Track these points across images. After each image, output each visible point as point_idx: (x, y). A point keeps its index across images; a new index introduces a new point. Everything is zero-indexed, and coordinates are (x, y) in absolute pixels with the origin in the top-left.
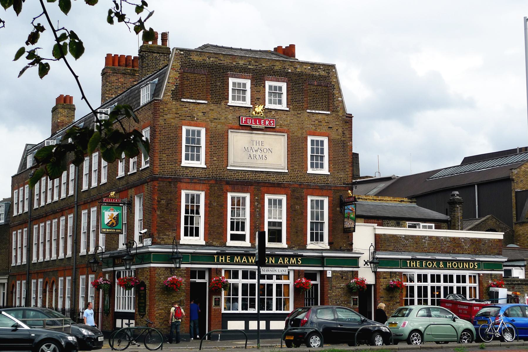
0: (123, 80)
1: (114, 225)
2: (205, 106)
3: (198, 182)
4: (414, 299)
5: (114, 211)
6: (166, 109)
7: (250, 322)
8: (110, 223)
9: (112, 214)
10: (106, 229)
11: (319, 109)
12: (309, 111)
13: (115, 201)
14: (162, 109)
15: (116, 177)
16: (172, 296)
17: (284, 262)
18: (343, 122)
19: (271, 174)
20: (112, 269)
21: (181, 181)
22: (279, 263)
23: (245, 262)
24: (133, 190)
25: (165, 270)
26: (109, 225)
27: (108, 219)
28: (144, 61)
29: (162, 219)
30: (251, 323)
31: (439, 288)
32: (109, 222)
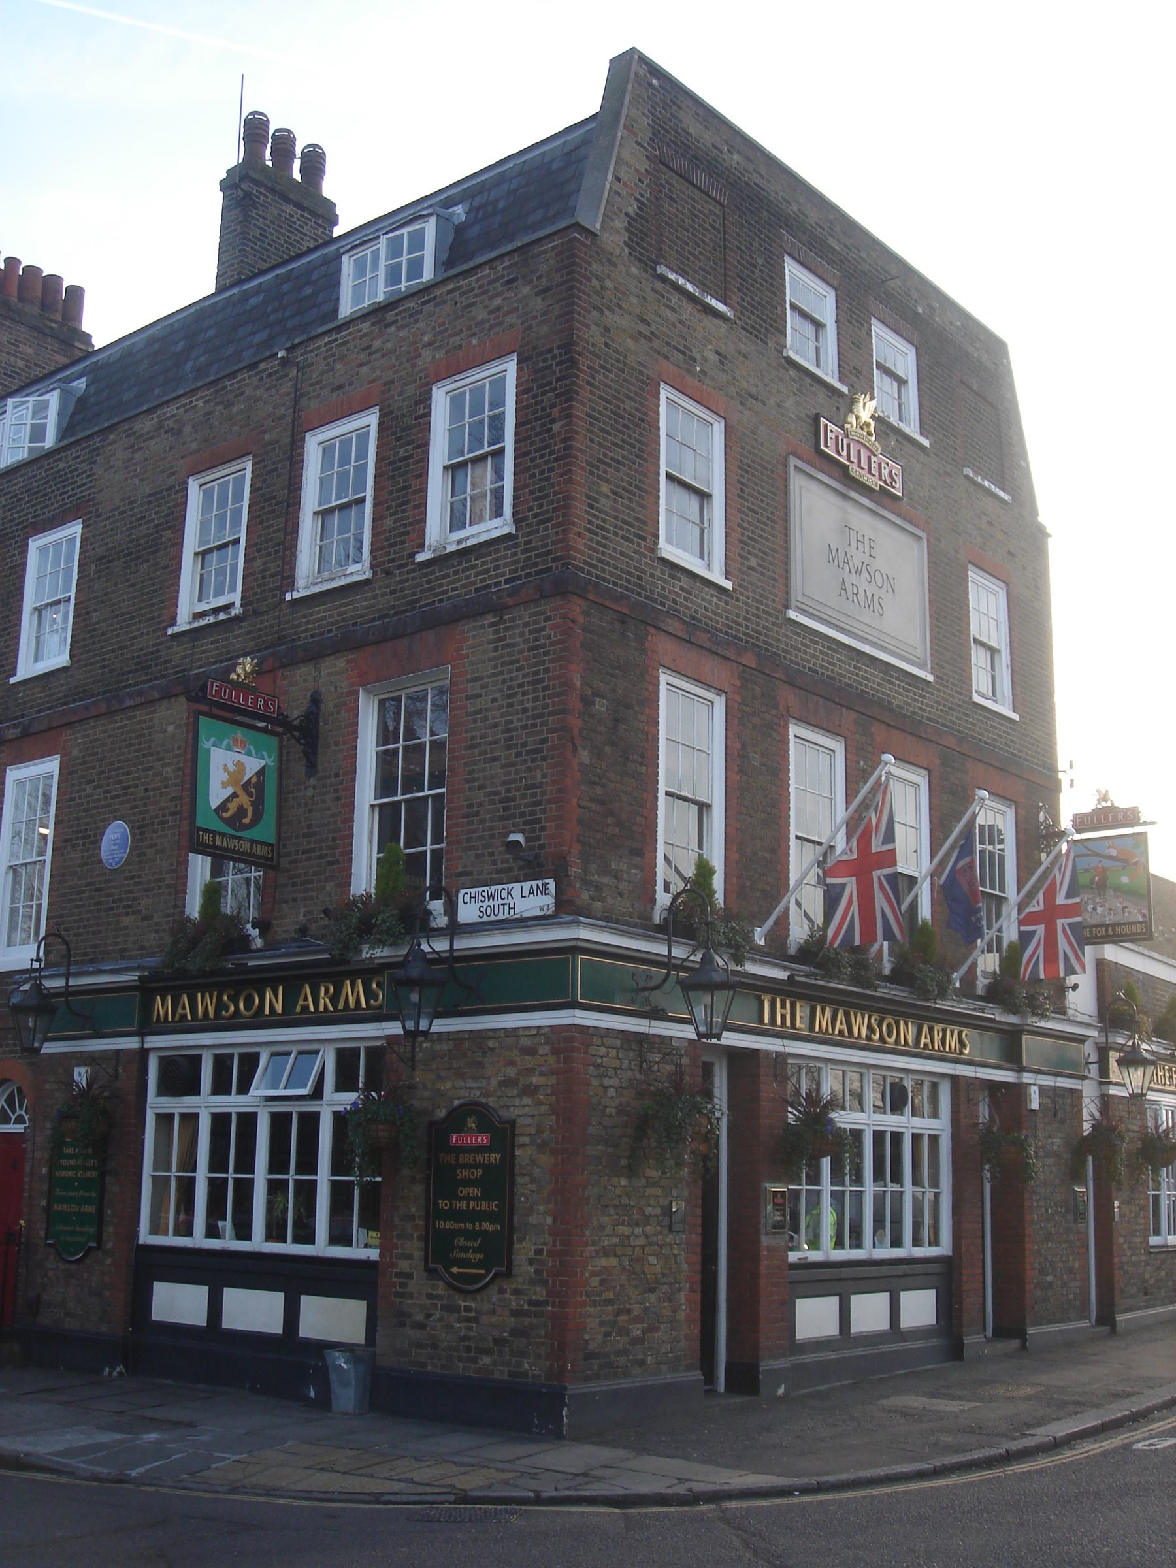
0: (30, 351)
1: (246, 821)
2: (724, 327)
3: (707, 645)
5: (249, 754)
6: (609, 284)
8: (230, 805)
9: (240, 766)
10: (214, 832)
11: (991, 477)
12: (968, 472)
13: (255, 702)
14: (597, 277)
15: (166, 628)
16: (643, 1181)
19: (892, 676)
20: (132, 1043)
21: (661, 625)
24: (340, 663)
25: (622, 1047)
26: (226, 815)
27: (224, 785)
28: (253, 218)
29: (598, 790)
30: (859, 1302)
31: (190, 1119)
32: (227, 800)
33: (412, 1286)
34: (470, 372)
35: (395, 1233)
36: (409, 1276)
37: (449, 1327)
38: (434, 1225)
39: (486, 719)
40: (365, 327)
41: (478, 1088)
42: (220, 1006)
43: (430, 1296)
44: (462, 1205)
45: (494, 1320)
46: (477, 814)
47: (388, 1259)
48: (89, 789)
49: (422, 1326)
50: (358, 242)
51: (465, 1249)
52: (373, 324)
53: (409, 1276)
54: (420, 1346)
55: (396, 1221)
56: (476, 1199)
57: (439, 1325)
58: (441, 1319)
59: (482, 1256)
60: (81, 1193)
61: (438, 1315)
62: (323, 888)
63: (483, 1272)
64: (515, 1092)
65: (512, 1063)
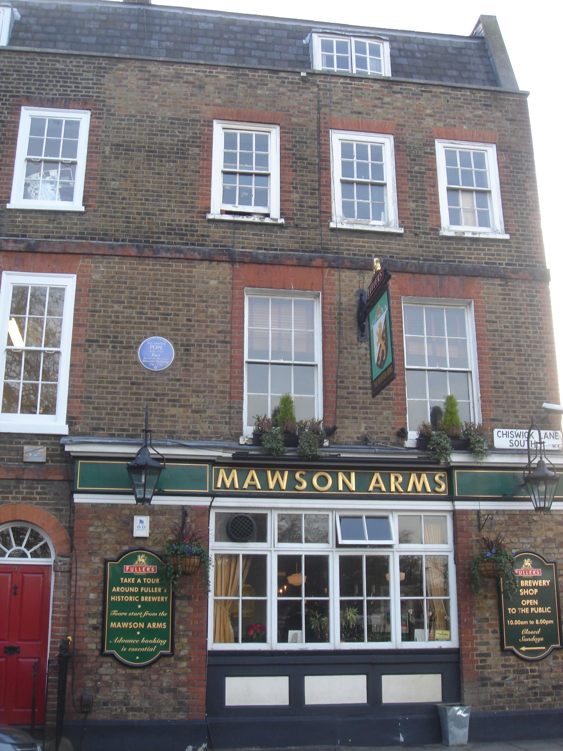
4: (342, 594)
7: (385, 678)
17: (388, 486)
18: (523, 214)
22: (371, 488)
23: (255, 486)
33: (490, 661)
34: (462, 142)
35: (474, 630)
36: (488, 655)
37: (520, 683)
38: (506, 623)
39: (502, 336)
40: (377, 86)
41: (529, 543)
42: (293, 482)
43: (504, 666)
44: (526, 610)
45: (552, 675)
46: (502, 387)
47: (470, 646)
48: (116, 307)
49: (500, 685)
50: (328, 31)
51: (527, 636)
52: (382, 87)
53: (488, 655)
54: (500, 696)
55: (475, 622)
56: (535, 606)
57: (513, 683)
58: (514, 679)
59: (542, 639)
60: (146, 614)
61: (512, 676)
62: (381, 413)
63: (544, 648)
64: (554, 546)
65: (550, 529)
